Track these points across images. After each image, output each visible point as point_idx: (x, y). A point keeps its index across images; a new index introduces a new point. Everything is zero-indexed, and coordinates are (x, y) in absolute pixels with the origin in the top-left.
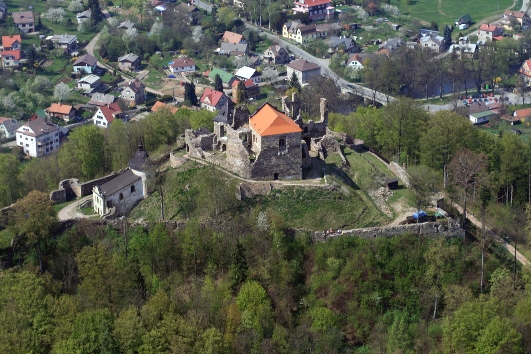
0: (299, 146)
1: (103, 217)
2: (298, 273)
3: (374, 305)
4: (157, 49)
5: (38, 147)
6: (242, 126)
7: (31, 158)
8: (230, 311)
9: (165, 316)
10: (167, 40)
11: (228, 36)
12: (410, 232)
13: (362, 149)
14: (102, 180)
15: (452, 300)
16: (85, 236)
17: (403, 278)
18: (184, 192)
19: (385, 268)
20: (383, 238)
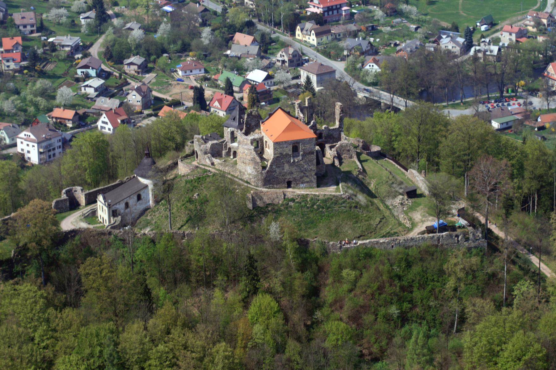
0: (313, 153)
1: (107, 227)
2: (312, 286)
3: (391, 319)
4: (164, 51)
5: (40, 153)
6: (253, 131)
7: (33, 165)
8: (241, 325)
9: (172, 331)
10: (174, 42)
11: (239, 37)
12: (429, 243)
13: (379, 156)
14: (106, 188)
15: (473, 314)
16: (89, 247)
17: (422, 291)
18: (193, 201)
19: (403, 280)
20: (401, 249)
